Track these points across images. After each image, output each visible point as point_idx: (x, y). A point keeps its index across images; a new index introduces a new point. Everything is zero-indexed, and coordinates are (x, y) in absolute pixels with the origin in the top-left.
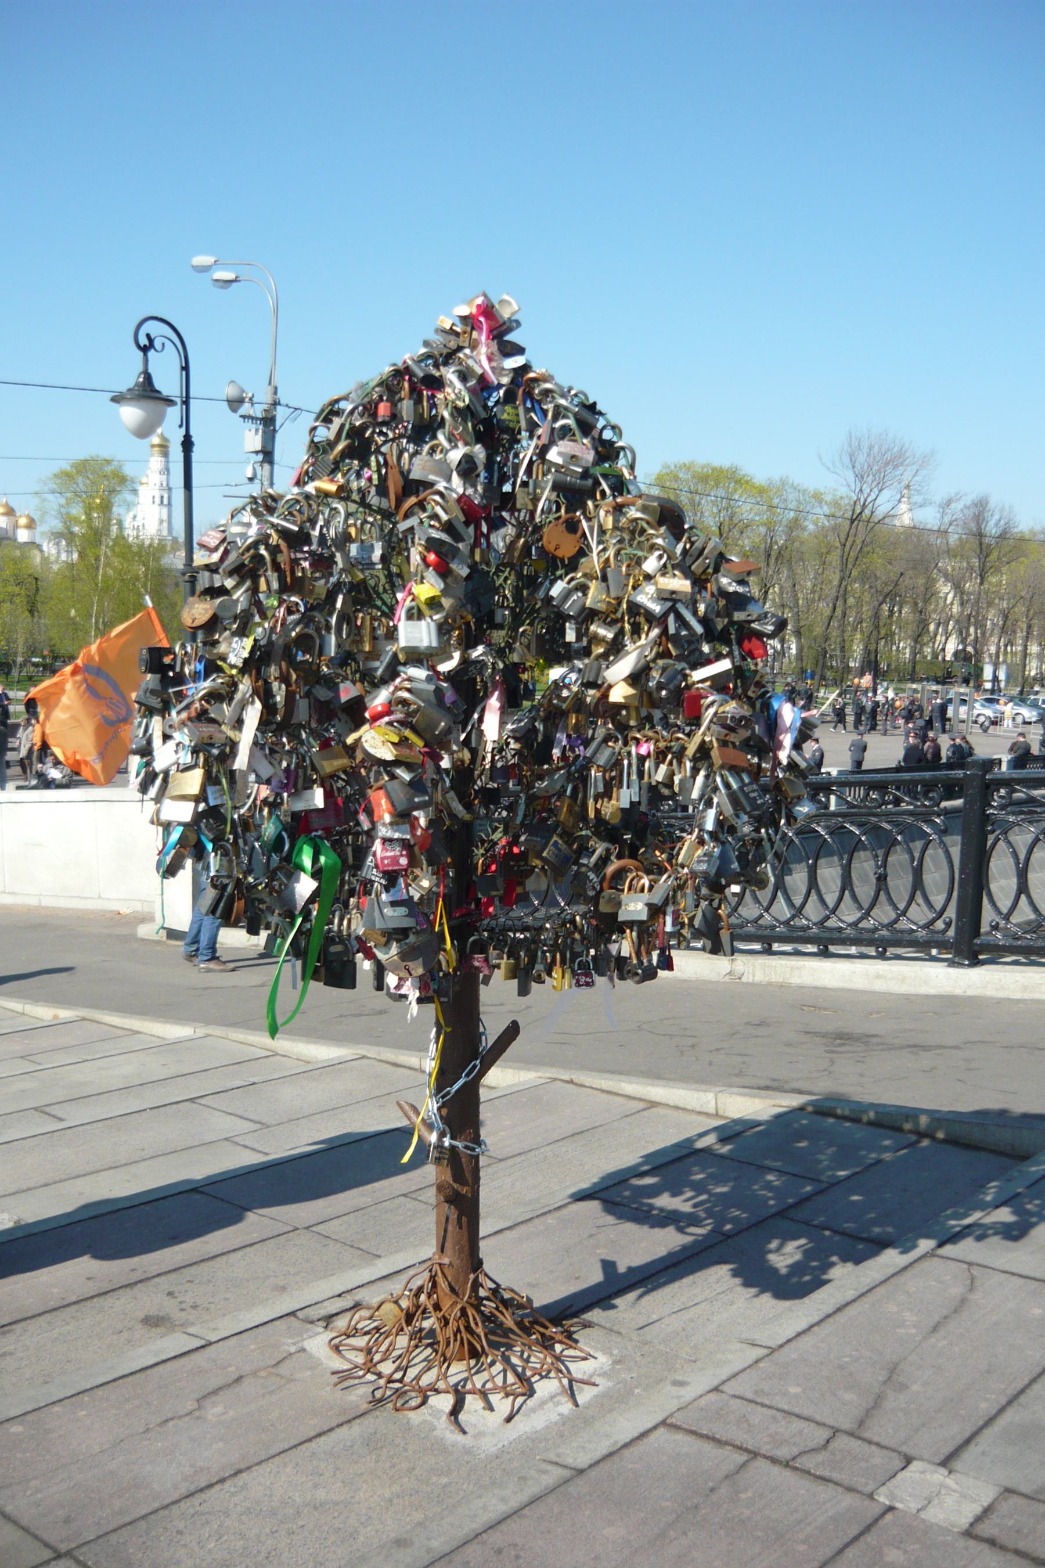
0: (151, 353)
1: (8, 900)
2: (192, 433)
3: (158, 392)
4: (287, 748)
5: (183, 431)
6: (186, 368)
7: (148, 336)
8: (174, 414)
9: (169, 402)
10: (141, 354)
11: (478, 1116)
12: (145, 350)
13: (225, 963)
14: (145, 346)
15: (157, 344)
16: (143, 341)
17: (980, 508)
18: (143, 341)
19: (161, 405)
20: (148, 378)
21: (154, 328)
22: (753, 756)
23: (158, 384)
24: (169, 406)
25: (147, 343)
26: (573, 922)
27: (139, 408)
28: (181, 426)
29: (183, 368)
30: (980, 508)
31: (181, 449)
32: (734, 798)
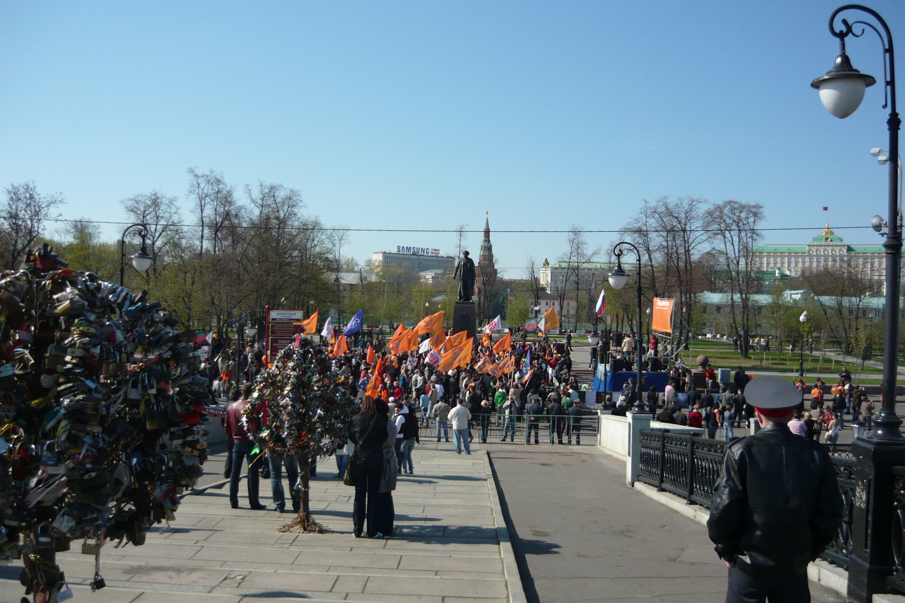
0: (849, 39)
1: (724, 597)
2: (897, 111)
3: (856, 71)
4: (334, 362)
5: (889, 110)
6: (890, 50)
7: (845, 22)
8: (875, 95)
9: (869, 81)
10: (837, 40)
11: (530, 576)
12: (841, 36)
13: (415, 476)
14: (841, 32)
15: (857, 29)
16: (839, 27)
17: (187, 172)
18: (839, 27)
19: (858, 84)
20: (846, 60)
21: (851, 16)
22: (332, 363)
23: (855, 65)
24: (868, 85)
25: (844, 29)
26: (111, 338)
27: (826, 88)
28: (885, 106)
29: (886, 51)
30: (187, 172)
31: (887, 127)
32: (244, 254)
